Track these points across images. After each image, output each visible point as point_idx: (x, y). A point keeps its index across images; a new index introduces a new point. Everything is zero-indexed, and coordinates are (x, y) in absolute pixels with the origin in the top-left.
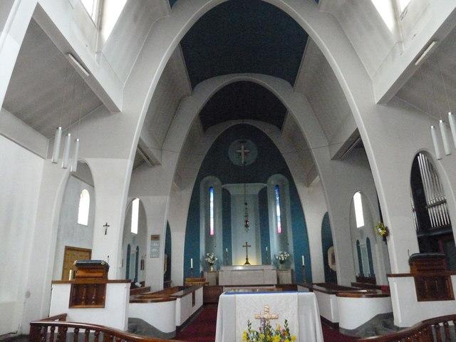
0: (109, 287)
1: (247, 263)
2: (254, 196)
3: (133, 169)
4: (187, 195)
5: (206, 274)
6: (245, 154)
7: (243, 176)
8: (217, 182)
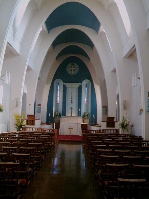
1: (71, 115)
6: (74, 70)
7: (77, 79)
8: (61, 83)
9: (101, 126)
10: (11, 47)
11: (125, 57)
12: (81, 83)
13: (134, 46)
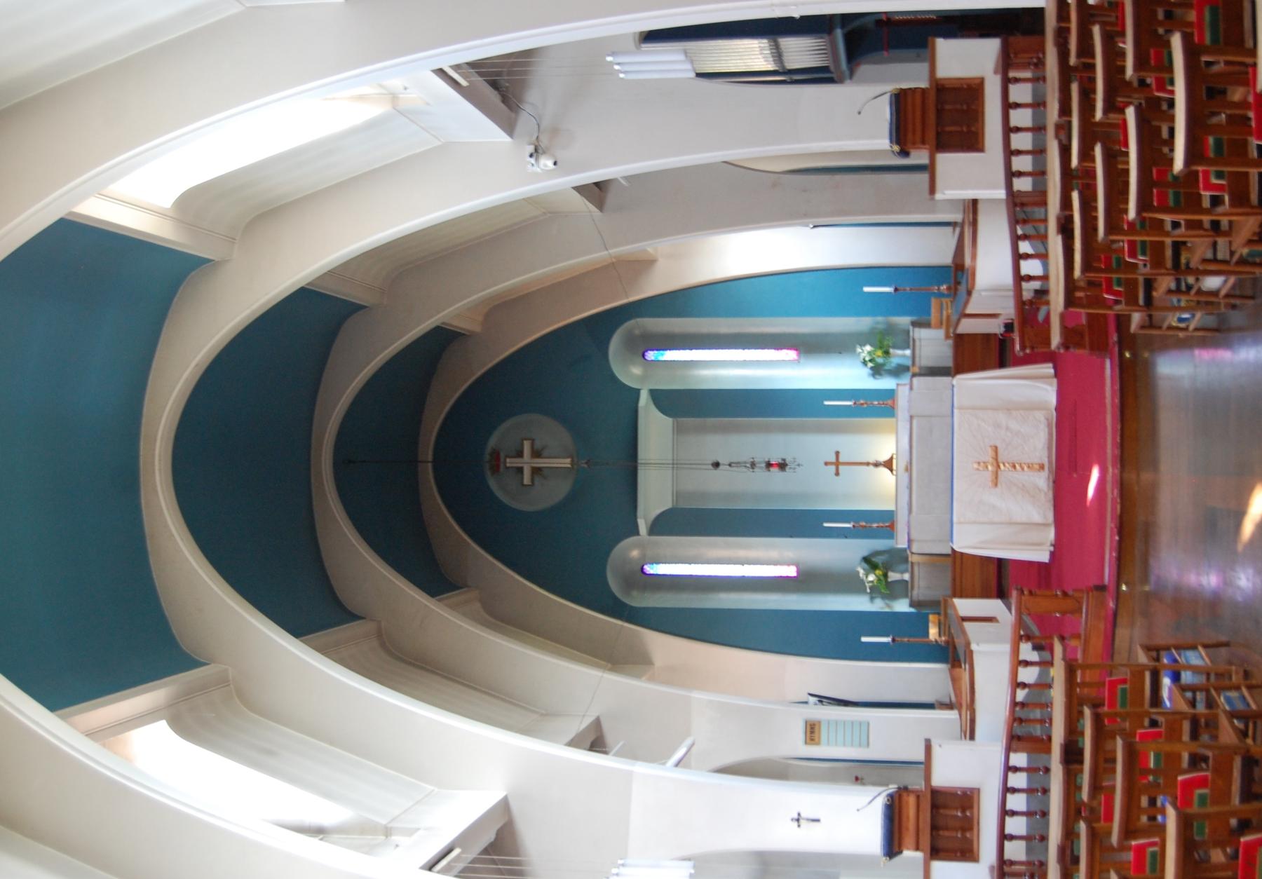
1: (888, 464)
2: (679, 430)
4: (662, 646)
5: (920, 592)
6: (536, 454)
8: (630, 550)
9: (975, 202)
10: (457, 851)
13: (441, 72)
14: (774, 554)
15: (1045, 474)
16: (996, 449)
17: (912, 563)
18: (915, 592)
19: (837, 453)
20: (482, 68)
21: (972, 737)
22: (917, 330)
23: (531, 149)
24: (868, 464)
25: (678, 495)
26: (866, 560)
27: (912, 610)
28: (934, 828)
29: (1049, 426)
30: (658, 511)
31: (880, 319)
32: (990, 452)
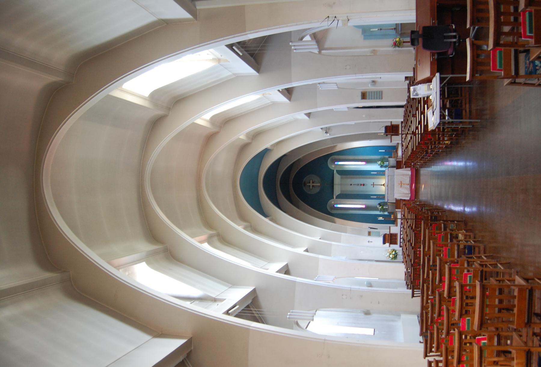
0: (392, 232)
2: (342, 178)
3: (264, 323)
5: (390, 210)
6: (313, 183)
8: (332, 202)
9: (398, 143)
11: (258, 70)
12: (334, 171)
14: (361, 203)
15: (409, 185)
16: (401, 182)
17: (388, 205)
18: (389, 210)
19: (374, 183)
20: (242, 45)
21: (397, 226)
22: (389, 159)
23: (325, 132)
24: (380, 185)
25: (341, 191)
26: (379, 204)
27: (388, 214)
28: (391, 239)
29: (410, 178)
30: (338, 194)
31: (382, 156)
32: (400, 182)
